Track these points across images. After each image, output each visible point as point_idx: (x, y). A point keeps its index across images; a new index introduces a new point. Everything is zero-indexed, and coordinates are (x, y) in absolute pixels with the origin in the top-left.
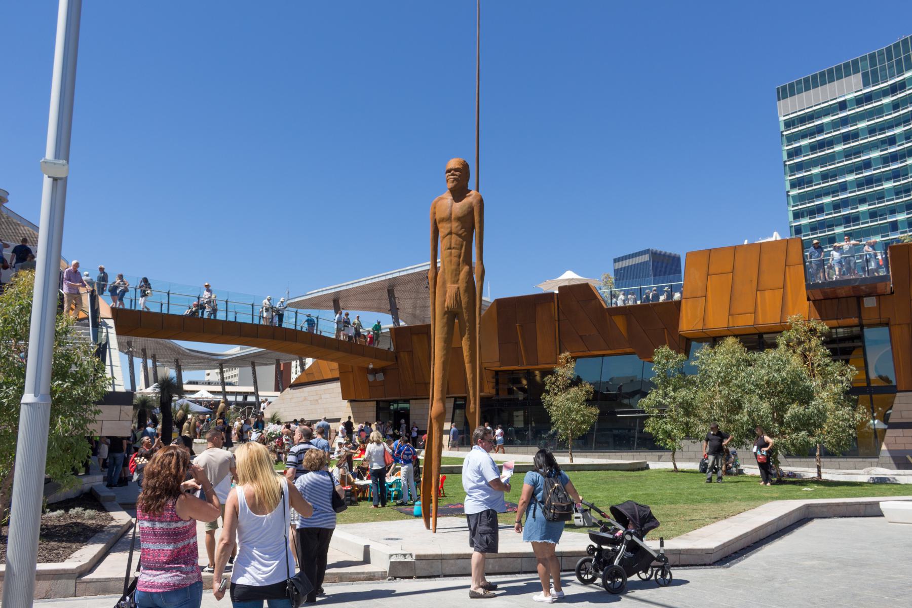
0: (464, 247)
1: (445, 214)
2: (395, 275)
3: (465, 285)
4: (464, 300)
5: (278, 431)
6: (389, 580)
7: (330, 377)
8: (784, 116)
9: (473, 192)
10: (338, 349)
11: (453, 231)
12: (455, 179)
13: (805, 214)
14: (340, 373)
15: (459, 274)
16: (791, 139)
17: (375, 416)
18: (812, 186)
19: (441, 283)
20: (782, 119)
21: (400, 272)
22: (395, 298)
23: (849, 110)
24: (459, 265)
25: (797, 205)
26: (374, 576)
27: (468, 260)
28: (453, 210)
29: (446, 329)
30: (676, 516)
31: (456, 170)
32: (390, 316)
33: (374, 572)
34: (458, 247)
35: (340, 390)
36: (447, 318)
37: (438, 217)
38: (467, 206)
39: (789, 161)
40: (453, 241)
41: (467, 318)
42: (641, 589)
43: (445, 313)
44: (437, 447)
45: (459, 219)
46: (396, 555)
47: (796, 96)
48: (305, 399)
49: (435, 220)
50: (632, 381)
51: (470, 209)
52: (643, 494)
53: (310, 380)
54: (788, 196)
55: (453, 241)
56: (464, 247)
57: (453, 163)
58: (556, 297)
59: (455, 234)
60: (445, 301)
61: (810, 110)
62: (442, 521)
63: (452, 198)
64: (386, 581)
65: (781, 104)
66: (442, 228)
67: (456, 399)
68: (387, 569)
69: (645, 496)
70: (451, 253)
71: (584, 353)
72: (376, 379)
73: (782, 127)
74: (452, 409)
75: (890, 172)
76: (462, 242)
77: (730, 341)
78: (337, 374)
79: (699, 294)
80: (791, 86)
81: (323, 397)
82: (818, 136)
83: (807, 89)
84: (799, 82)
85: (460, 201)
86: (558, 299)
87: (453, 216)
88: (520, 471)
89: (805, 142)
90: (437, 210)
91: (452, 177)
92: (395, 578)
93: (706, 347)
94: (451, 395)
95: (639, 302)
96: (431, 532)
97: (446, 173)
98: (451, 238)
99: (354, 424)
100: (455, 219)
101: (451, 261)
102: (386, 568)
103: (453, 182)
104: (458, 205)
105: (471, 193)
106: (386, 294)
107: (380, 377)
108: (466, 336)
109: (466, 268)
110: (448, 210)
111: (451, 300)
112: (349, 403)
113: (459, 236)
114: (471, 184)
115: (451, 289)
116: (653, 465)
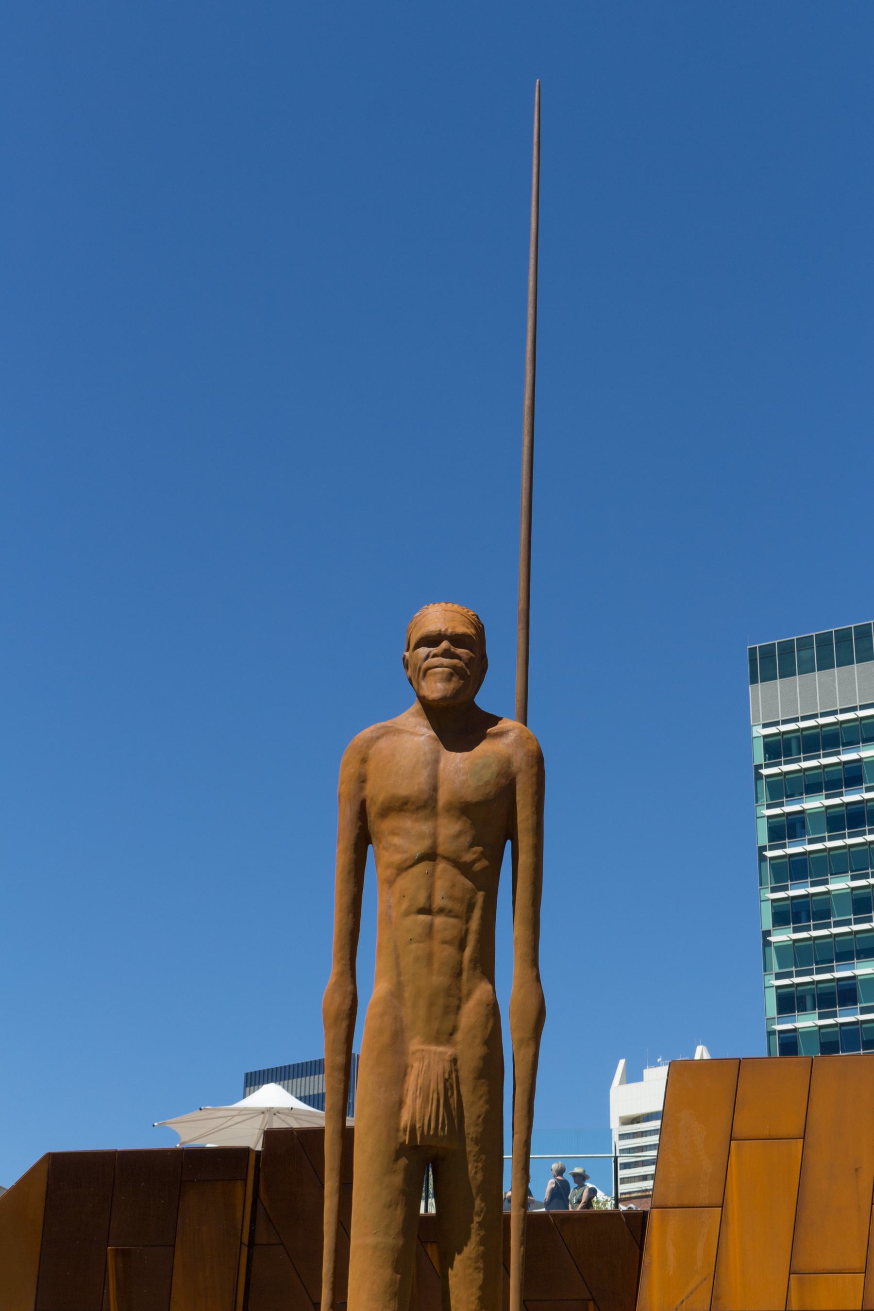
8: (765, 726)
9: (509, 723)
11: (441, 850)
13: (809, 1002)
15: (459, 1008)
18: (827, 926)
20: (759, 731)
25: (789, 975)
28: (442, 775)
31: (457, 640)
34: (458, 907)
36: (407, 1169)
38: (494, 768)
41: (480, 1176)
43: (401, 1151)
51: (503, 781)
54: (767, 944)
59: (447, 859)
60: (401, 1103)
61: (851, 716)
65: (758, 692)
66: (394, 833)
70: (431, 926)
80: (786, 648)
83: (825, 664)
84: (805, 643)
86: (257, 1169)
87: (443, 797)
89: (814, 803)
90: (371, 767)
98: (431, 874)
101: (430, 957)
103: (449, 678)
105: (501, 726)
108: (471, 1249)
111: (426, 1101)
113: (464, 868)
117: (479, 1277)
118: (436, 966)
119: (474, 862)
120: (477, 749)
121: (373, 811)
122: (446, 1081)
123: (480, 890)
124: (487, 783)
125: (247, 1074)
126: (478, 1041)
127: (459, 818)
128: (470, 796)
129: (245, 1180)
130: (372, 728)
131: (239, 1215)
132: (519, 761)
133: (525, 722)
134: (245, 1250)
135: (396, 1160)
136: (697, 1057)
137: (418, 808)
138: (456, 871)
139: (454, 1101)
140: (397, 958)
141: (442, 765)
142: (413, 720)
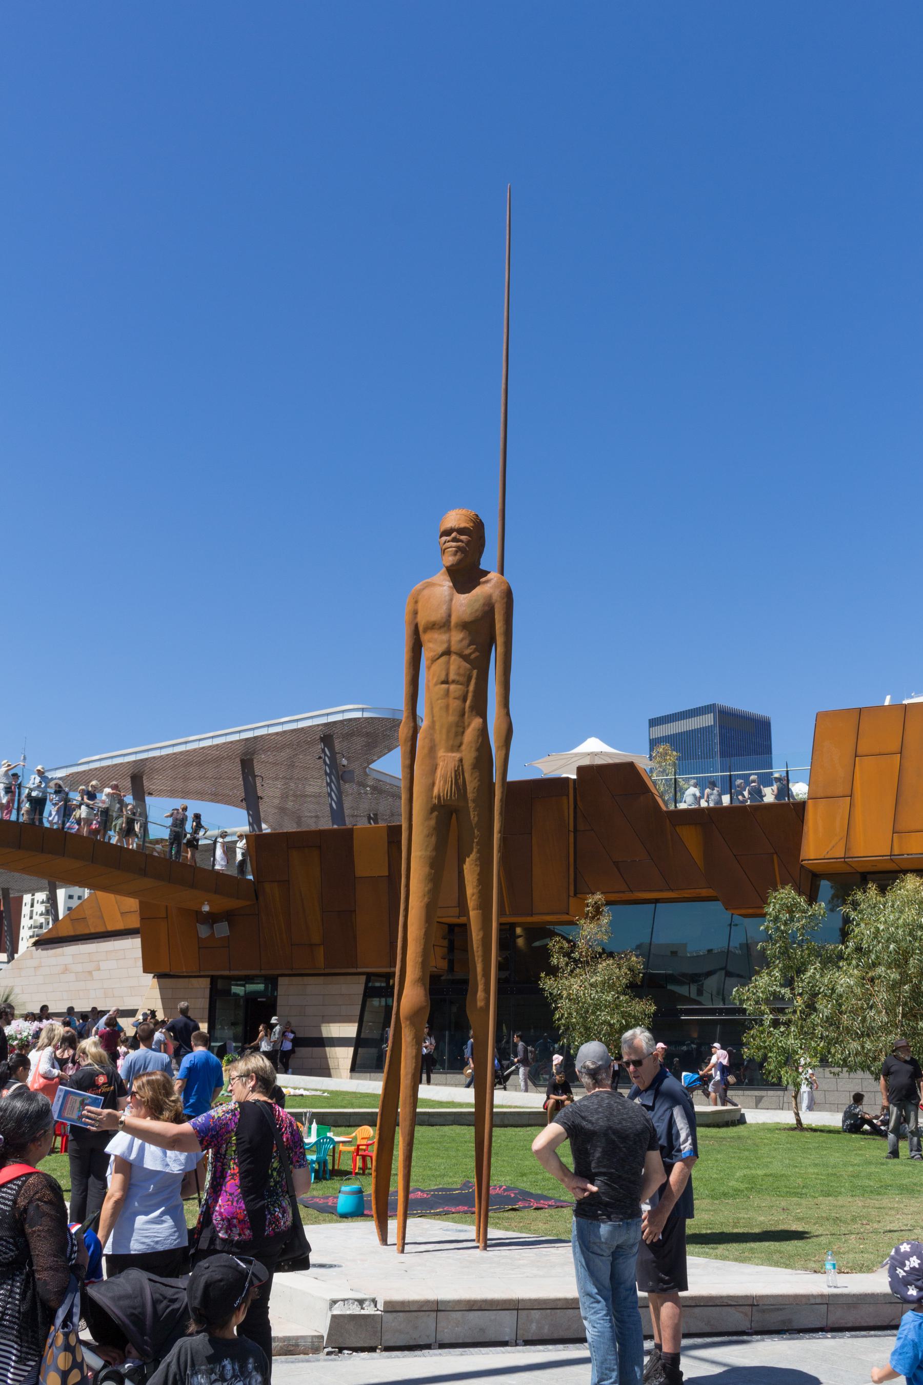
0: (473, 682)
1: (438, 615)
2: (258, 733)
3: (473, 754)
4: (472, 784)
5: (25, 1034)
6: (329, 1353)
7: (120, 926)
9: (494, 576)
10: (144, 873)
11: (453, 649)
12: (459, 549)
14: (142, 919)
15: (463, 733)
17: (207, 1006)
19: (426, 751)
21: (268, 726)
22: (255, 776)
24: (463, 714)
26: (297, 1345)
27: (480, 708)
28: (454, 608)
29: (433, 839)
30: (854, 1220)
31: (461, 531)
32: (244, 813)
33: (298, 1338)
34: (461, 679)
35: (139, 953)
36: (437, 817)
37: (422, 620)
38: (481, 602)
40: (453, 668)
41: (476, 819)
42: (268, 1299)
43: (433, 809)
44: (410, 1076)
45: (465, 626)
46: (344, 1300)
48: (66, 970)
49: (416, 626)
50: (674, 953)
51: (487, 608)
52: (766, 1175)
53: (78, 933)
55: (453, 668)
56: (473, 682)
57: (454, 518)
58: (571, 785)
59: (455, 653)
60: (433, 784)
62: (419, 1228)
63: (451, 584)
64: (322, 1356)
66: (429, 641)
67: (369, 976)
68: (324, 1331)
69: (771, 1179)
70: (448, 690)
71: (621, 895)
72: (213, 933)
74: (361, 997)
76: (471, 671)
78: (134, 922)
79: (840, 791)
81: (103, 965)
85: (469, 592)
86: (575, 789)
87: (454, 620)
88: (506, 1122)
90: (420, 605)
91: (454, 544)
92: (341, 1350)
93: (872, 889)
94: (359, 970)
95: (704, 804)
96: (392, 1252)
97: (441, 537)
98: (448, 663)
100: (457, 625)
102: (322, 1327)
103: (455, 554)
104: (462, 600)
105: (489, 576)
106: (236, 768)
107: (222, 929)
108: (473, 856)
109: (477, 722)
110: (445, 607)
111: (445, 782)
112: (156, 980)
113: (465, 658)
114: (488, 560)
115: (446, 761)
116: (754, 1116)
117: (478, 869)
118: (451, 711)
119: (471, 654)
120: (474, 592)
121: (421, 629)
122: (456, 771)
123: (474, 669)
124: (477, 611)
125: (650, 720)
126: (473, 749)
127: (462, 631)
128: (467, 618)
129: (568, 796)
130: (421, 583)
131: (566, 814)
132: (497, 595)
133: (502, 574)
134: (572, 835)
135: (431, 813)
136: (887, 703)
137: (441, 627)
138: (461, 660)
139: (460, 781)
140: (432, 708)
141: (454, 602)
142: (442, 577)
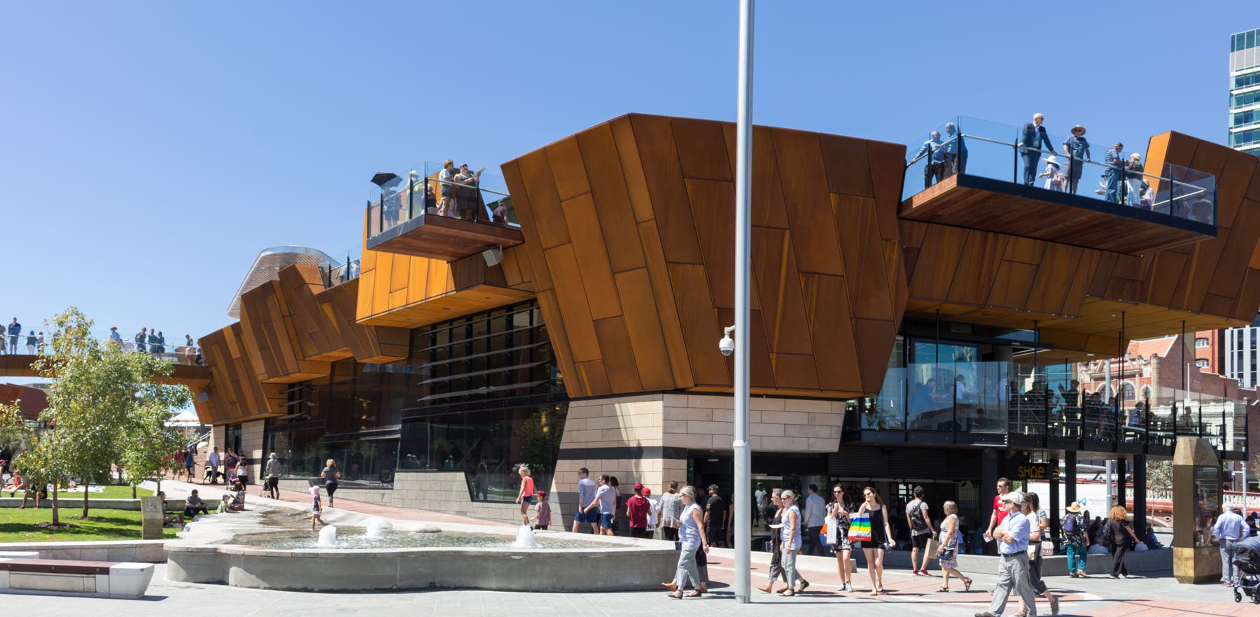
16: (1242, 100)
20: (1233, 74)
23: (1255, 124)
39: (1235, 128)
47: (1255, 48)
73: (1233, 84)
75: (730, 472)
77: (661, 494)
82: (1245, 126)
99: (726, 336)
